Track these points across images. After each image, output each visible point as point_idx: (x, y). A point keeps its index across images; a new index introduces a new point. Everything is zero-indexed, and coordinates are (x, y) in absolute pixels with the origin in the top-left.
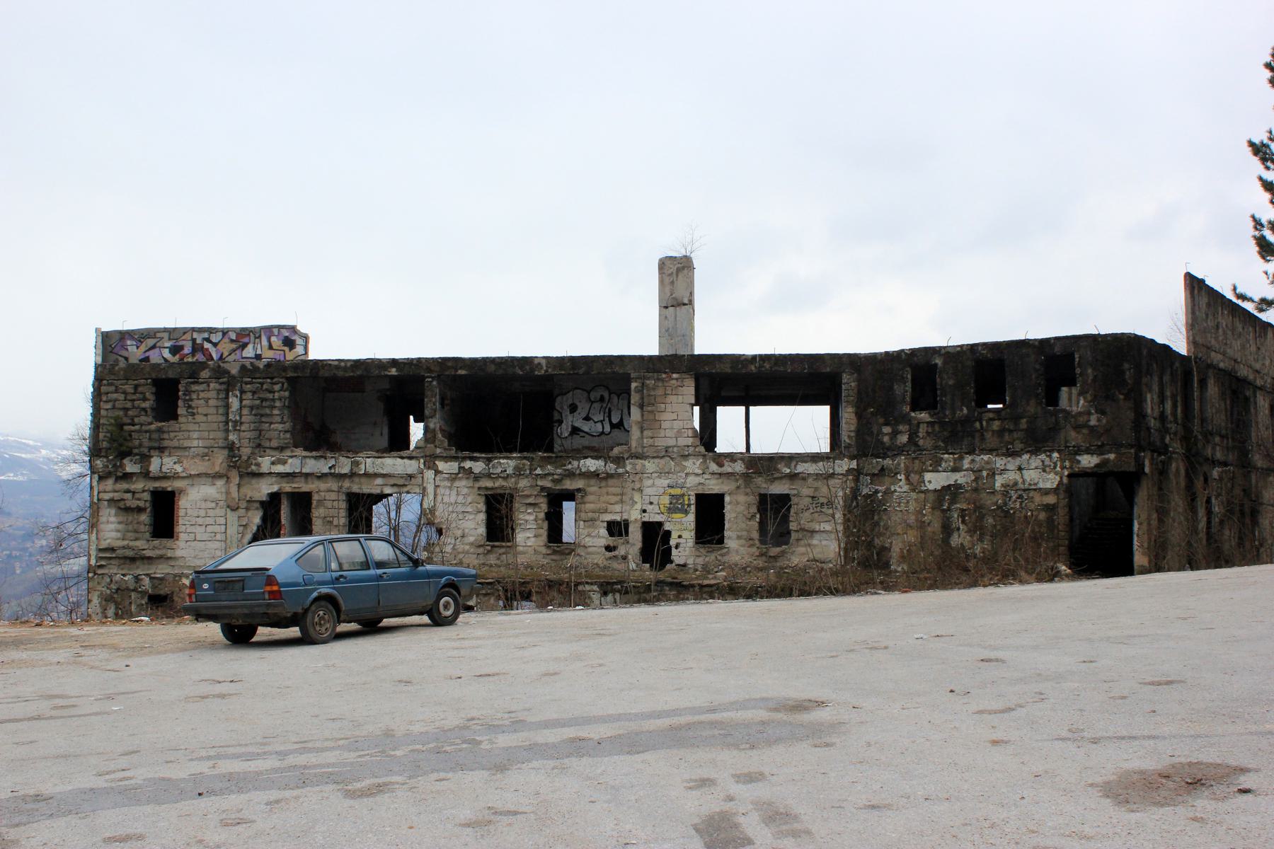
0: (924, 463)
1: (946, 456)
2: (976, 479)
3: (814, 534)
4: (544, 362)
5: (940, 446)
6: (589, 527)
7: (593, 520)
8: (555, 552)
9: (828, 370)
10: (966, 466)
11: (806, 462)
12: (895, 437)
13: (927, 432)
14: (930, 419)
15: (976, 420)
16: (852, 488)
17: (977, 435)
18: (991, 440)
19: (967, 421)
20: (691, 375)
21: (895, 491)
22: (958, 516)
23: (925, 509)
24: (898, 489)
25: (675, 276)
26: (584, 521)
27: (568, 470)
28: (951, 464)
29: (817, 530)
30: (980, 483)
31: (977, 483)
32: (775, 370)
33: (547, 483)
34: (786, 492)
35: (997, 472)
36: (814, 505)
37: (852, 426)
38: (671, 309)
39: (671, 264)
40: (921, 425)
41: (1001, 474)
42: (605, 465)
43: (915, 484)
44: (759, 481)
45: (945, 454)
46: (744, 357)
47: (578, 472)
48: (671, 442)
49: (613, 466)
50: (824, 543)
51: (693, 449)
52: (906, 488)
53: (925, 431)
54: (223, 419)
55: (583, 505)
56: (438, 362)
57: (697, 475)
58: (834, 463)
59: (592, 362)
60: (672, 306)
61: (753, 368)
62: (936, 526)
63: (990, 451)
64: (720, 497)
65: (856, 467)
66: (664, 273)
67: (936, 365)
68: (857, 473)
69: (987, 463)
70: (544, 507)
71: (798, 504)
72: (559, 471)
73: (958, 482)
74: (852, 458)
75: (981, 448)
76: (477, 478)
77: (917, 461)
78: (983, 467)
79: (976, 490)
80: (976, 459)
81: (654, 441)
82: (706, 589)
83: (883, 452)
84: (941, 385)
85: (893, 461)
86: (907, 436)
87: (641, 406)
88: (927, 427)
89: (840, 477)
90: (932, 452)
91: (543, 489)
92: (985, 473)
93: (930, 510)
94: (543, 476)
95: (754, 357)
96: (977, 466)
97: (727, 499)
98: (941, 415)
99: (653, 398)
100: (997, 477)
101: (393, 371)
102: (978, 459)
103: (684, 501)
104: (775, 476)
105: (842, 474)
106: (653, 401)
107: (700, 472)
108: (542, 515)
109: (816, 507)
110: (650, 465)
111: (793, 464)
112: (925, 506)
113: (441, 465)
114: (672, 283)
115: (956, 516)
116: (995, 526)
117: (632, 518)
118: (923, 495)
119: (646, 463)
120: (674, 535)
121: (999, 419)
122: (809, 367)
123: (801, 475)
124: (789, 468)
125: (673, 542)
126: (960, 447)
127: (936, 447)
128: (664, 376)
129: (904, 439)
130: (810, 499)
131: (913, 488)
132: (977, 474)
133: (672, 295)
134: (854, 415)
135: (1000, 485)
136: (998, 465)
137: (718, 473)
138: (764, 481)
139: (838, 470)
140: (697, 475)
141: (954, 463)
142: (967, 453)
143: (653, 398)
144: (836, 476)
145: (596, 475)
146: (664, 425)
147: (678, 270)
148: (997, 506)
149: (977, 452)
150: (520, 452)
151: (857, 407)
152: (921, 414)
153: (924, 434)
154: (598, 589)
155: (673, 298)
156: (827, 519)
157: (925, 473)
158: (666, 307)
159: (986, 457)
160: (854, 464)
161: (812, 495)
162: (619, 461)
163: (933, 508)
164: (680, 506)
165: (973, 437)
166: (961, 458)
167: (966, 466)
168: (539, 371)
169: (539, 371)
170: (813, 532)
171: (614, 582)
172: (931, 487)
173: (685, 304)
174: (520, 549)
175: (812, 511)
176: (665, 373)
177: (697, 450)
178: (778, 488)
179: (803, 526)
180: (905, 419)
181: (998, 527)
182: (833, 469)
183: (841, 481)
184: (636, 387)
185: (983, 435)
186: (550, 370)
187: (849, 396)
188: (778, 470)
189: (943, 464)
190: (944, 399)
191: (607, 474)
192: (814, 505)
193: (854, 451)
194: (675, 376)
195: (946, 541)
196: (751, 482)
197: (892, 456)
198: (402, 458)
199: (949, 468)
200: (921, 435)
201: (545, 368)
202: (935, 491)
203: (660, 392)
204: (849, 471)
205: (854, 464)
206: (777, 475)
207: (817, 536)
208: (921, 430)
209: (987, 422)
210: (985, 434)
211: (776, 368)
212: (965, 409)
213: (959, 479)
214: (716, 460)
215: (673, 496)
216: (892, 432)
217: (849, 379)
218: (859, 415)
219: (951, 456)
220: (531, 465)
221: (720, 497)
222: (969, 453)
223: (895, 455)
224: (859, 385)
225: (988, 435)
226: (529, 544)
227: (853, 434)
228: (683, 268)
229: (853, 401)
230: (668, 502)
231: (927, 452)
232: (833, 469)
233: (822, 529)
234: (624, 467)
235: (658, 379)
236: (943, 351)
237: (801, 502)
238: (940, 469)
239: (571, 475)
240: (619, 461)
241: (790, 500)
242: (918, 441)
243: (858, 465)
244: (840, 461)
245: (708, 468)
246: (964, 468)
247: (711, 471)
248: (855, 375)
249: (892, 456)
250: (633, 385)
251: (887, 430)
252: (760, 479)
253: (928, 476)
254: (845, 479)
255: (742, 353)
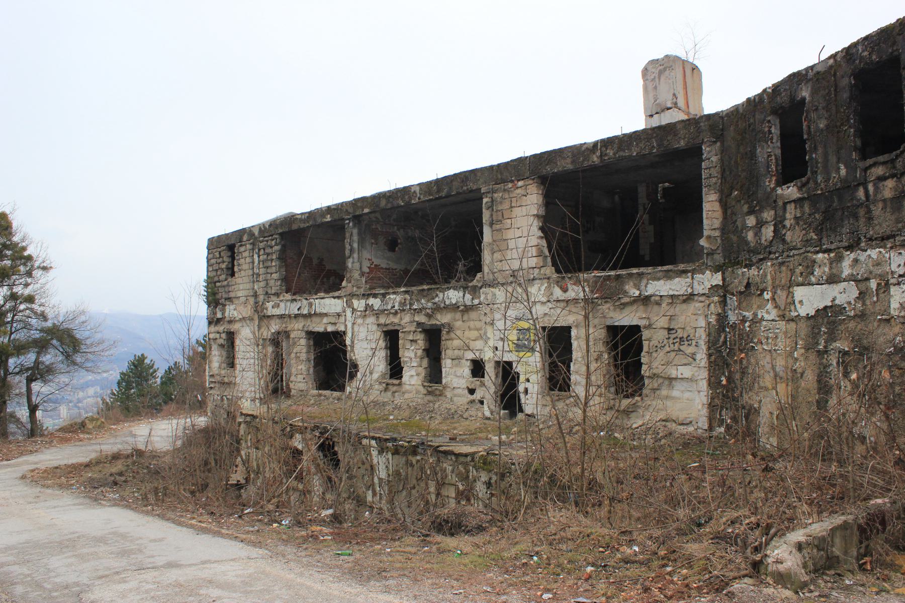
0: (792, 271)
1: (820, 255)
2: (862, 295)
3: (674, 382)
4: (417, 189)
5: (811, 239)
6: (457, 366)
7: (459, 358)
8: (429, 393)
9: (682, 143)
10: (846, 272)
11: (659, 279)
12: (760, 230)
13: (796, 218)
14: (799, 195)
15: (859, 185)
16: (719, 315)
17: (862, 212)
18: (884, 221)
19: (848, 187)
20: (534, 179)
21: (762, 319)
22: (838, 363)
23: (796, 350)
24: (766, 317)
25: (657, 80)
26: (453, 359)
27: (435, 303)
28: (827, 269)
29: (674, 376)
30: (868, 302)
31: (864, 304)
32: (619, 157)
33: (421, 318)
34: (634, 323)
35: (892, 281)
36: (671, 341)
37: (715, 221)
38: (656, 116)
39: (653, 68)
40: (788, 207)
41: (899, 284)
42: (464, 296)
43: (783, 308)
44: (605, 307)
45: (817, 252)
46: (585, 146)
47: (442, 305)
48: (516, 265)
49: (468, 296)
50: (687, 395)
51: (538, 270)
52: (773, 314)
53: (792, 216)
54: (251, 272)
55: (450, 342)
56: (353, 204)
57: (543, 303)
58: (693, 278)
59: (452, 181)
60: (657, 113)
61: (595, 159)
62: (810, 377)
63: (882, 240)
64: (568, 329)
65: (721, 283)
66: (647, 80)
67: (804, 99)
68: (723, 291)
69: (878, 264)
70: (421, 344)
71: (652, 338)
72: (430, 304)
73: (837, 302)
74: (717, 269)
75: (868, 236)
76: (378, 314)
77: (784, 268)
78: (871, 272)
79: (862, 316)
80: (859, 258)
81: (502, 265)
82: (462, 459)
83: (761, 254)
84: (809, 133)
85: (759, 269)
86: (772, 228)
87: (491, 224)
88: (796, 208)
89: (701, 299)
90: (802, 251)
91: (419, 324)
92: (873, 284)
93: (803, 351)
94: (419, 311)
95: (595, 144)
96: (861, 271)
97: (574, 333)
98: (811, 185)
99: (500, 213)
100: (893, 290)
101: (328, 218)
102: (863, 256)
103: (530, 336)
104: (623, 301)
105: (704, 294)
106: (500, 218)
107: (544, 299)
108: (420, 352)
109: (674, 343)
110: (500, 294)
111: (644, 282)
112: (796, 344)
113: (355, 303)
114: (655, 88)
115: (834, 363)
116: (892, 385)
117: (486, 358)
118: (792, 325)
119: (496, 291)
120: (522, 378)
121: (892, 176)
122: (658, 145)
123: (653, 298)
124: (638, 289)
125: (521, 388)
126: (838, 238)
127: (807, 242)
128: (510, 185)
129: (768, 232)
130: (666, 332)
131: (781, 313)
132: (863, 286)
133: (655, 101)
134: (718, 204)
135: (897, 305)
136: (894, 267)
137: (563, 301)
138: (612, 308)
139: (699, 289)
140: (543, 303)
141: (831, 268)
142: (848, 248)
143: (500, 213)
144: (696, 298)
145: (455, 307)
146: (512, 244)
147: (661, 73)
148: (895, 347)
149: (863, 244)
150: (406, 285)
151: (721, 192)
152: (788, 187)
153: (792, 221)
154: (376, 446)
155: (657, 104)
156: (685, 361)
157: (795, 288)
158: (651, 116)
159: (874, 253)
160: (717, 279)
161: (666, 326)
162: (475, 291)
163: (807, 349)
164: (526, 343)
165: (856, 217)
166: (840, 259)
167: (846, 272)
168: (415, 200)
169: (415, 200)
170: (671, 379)
171: (388, 439)
172: (803, 311)
173: (668, 109)
174: (407, 387)
175: (667, 349)
176: (512, 181)
177: (542, 272)
178: (627, 318)
179: (655, 371)
180: (771, 201)
181: (897, 389)
182: (692, 288)
183: (702, 304)
184: (487, 203)
185: (869, 211)
186: (422, 197)
187: (710, 176)
188: (625, 293)
189: (817, 272)
190: (814, 156)
191: (465, 306)
192: (671, 341)
193: (719, 258)
194: (520, 183)
195: (822, 404)
196: (598, 311)
197: (757, 262)
198: (334, 298)
199: (825, 278)
200: (787, 223)
201: (418, 195)
202: (808, 318)
203: (506, 205)
204: (714, 288)
205: (717, 279)
206: (626, 300)
207: (678, 385)
208: (788, 216)
209: (874, 185)
210: (871, 206)
211: (621, 153)
212: (842, 167)
213: (838, 296)
214: (560, 284)
215: (520, 330)
216: (757, 224)
217: (709, 152)
218: (724, 204)
219: (826, 255)
220: (411, 299)
221: (568, 329)
222: (850, 248)
223: (761, 260)
224: (722, 160)
225: (877, 210)
226: (412, 383)
227: (717, 233)
228: (665, 69)
229: (716, 183)
230: (516, 338)
231: (796, 252)
232: (692, 288)
233: (680, 376)
234: (479, 297)
235: (505, 190)
236: (811, 73)
237: (655, 337)
238: (813, 279)
239: (437, 309)
240: (475, 291)
241: (640, 331)
242: (784, 235)
243: (724, 279)
244: (701, 276)
245: (552, 294)
246: (843, 276)
247: (555, 298)
248: (718, 144)
249: (757, 262)
250: (485, 200)
251: (751, 221)
252: (608, 305)
253: (799, 292)
254: (707, 302)
255: (583, 142)
